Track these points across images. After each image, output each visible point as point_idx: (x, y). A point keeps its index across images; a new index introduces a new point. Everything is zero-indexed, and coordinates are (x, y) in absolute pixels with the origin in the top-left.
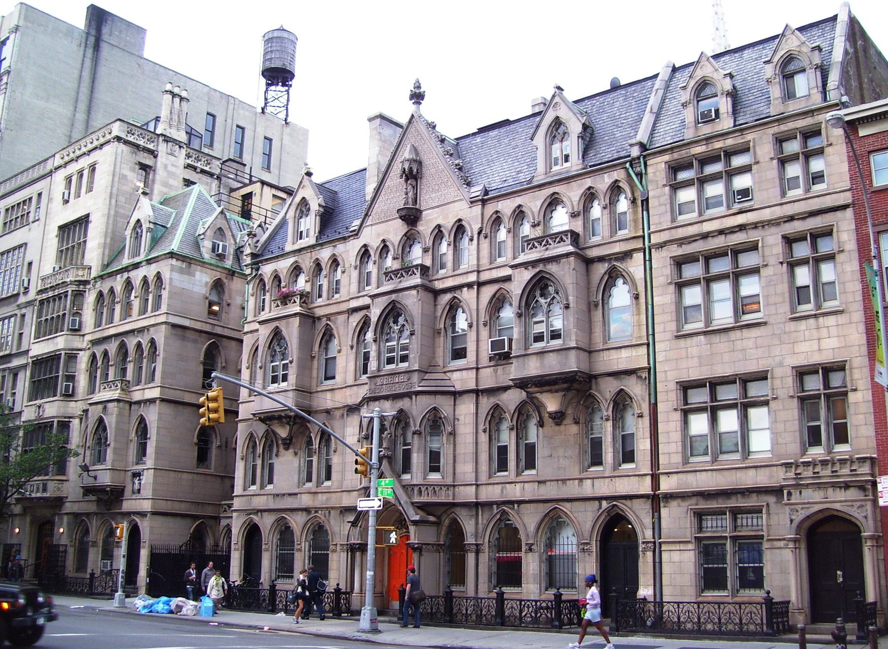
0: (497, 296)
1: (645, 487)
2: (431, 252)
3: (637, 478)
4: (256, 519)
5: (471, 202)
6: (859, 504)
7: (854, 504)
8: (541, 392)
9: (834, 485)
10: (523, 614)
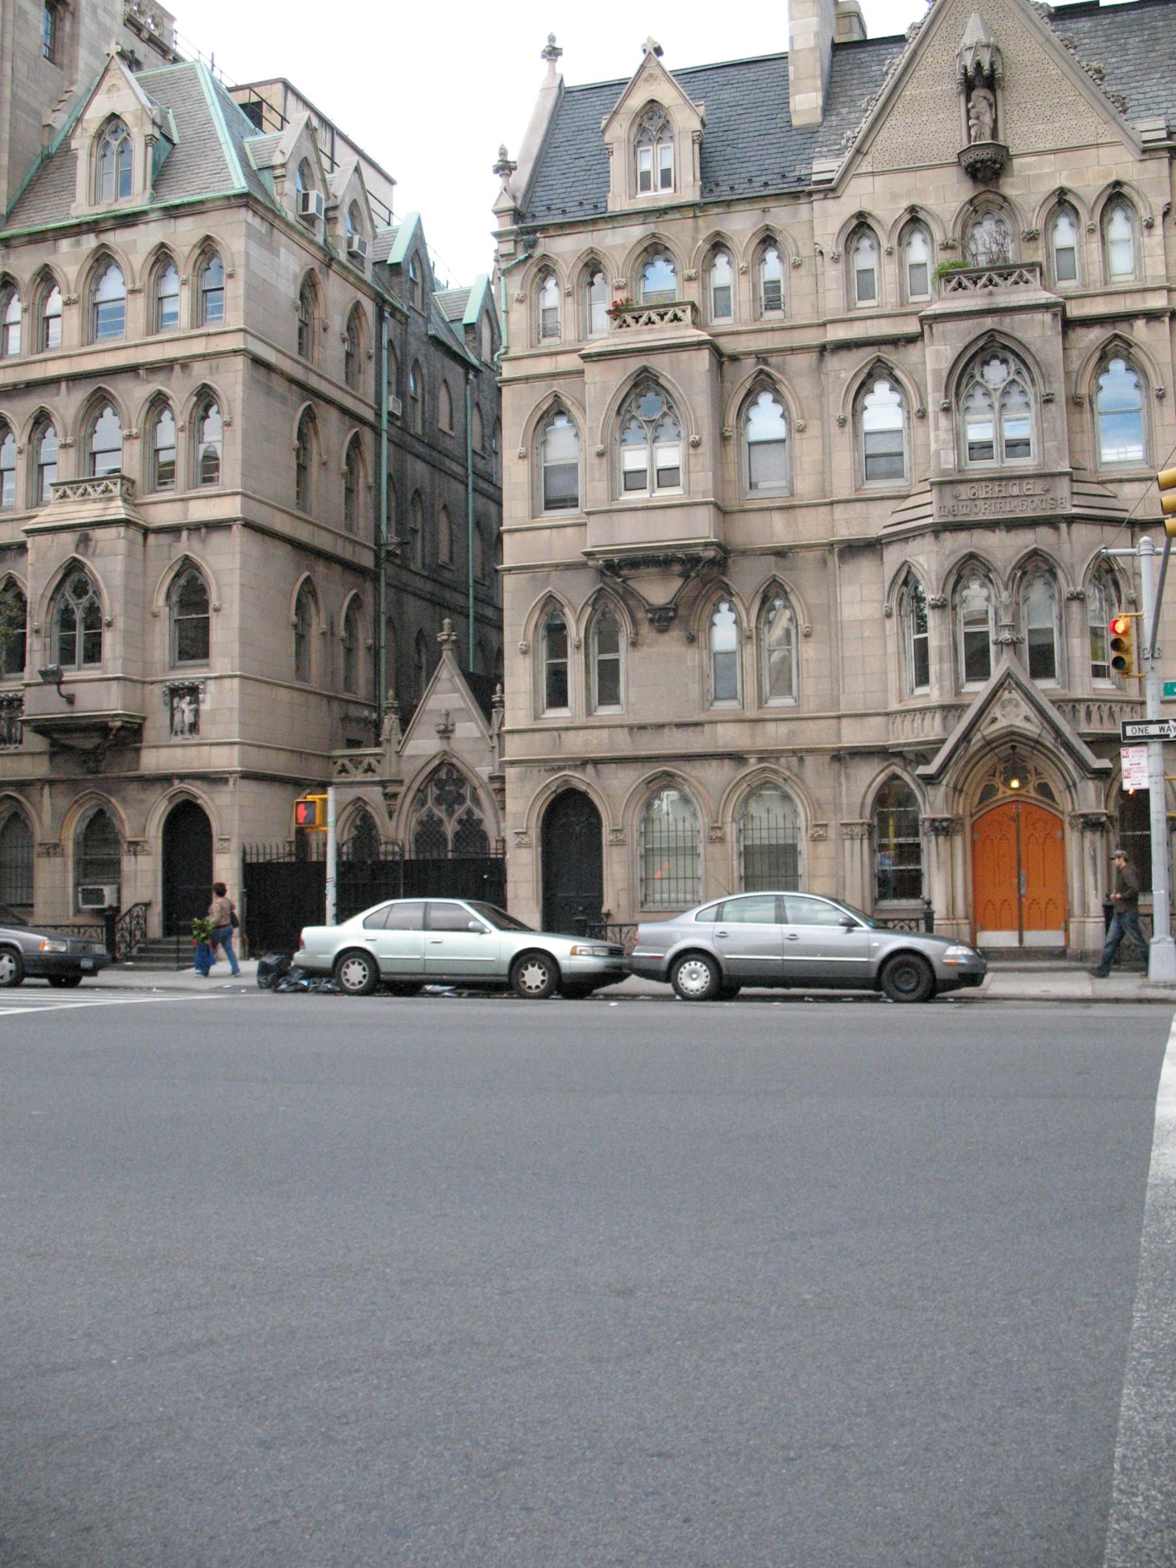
2: (1098, 233)
4: (582, 780)
5: (1144, 151)
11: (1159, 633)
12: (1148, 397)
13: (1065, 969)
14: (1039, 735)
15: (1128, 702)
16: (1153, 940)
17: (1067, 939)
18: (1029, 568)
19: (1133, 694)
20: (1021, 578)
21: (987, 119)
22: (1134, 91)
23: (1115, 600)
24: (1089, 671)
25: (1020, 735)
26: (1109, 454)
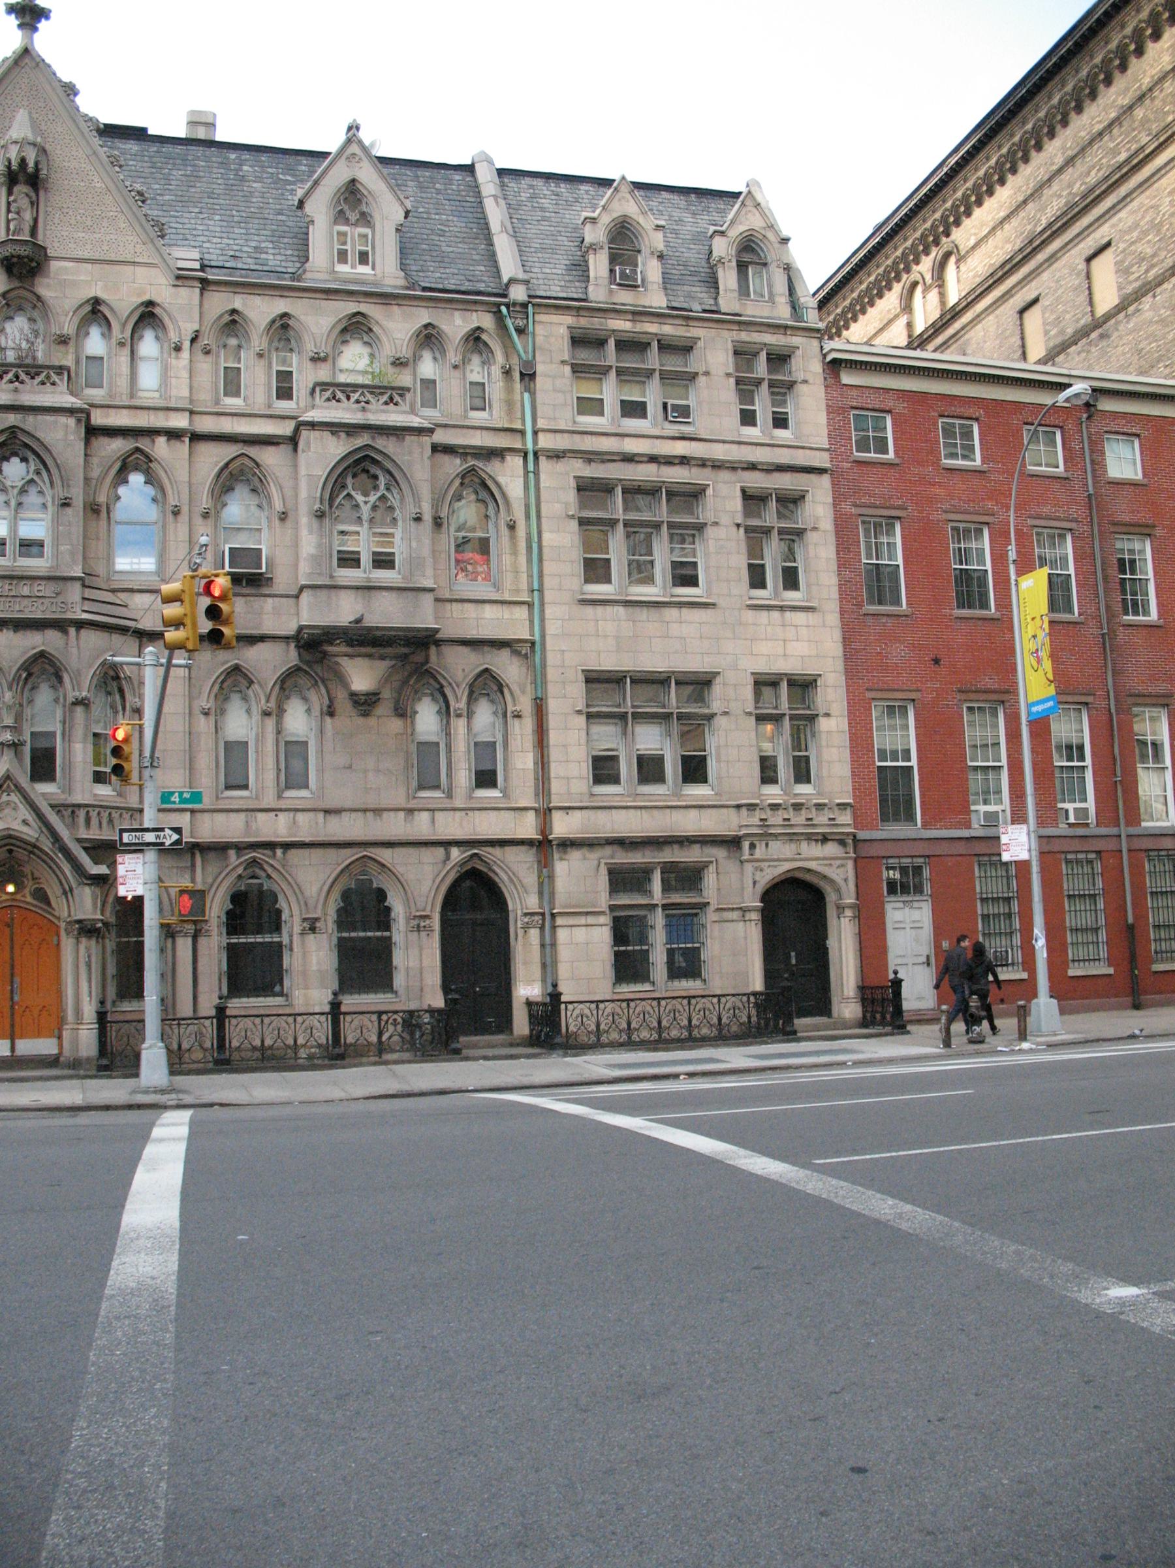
0: (232, 466)
1: (527, 827)
3: (512, 813)
5: (178, 277)
6: (839, 862)
7: (832, 862)
8: (351, 656)
9: (810, 837)
10: (384, 1038)
11: (159, 742)
12: (164, 512)
13: (57, 1078)
14: (37, 839)
15: (128, 809)
16: (144, 1046)
17: (61, 1046)
18: (35, 669)
19: (133, 802)
20: (26, 679)
21: (28, 216)
22: (173, 220)
23: (120, 708)
24: (90, 777)
25: (17, 838)
26: (123, 563)
